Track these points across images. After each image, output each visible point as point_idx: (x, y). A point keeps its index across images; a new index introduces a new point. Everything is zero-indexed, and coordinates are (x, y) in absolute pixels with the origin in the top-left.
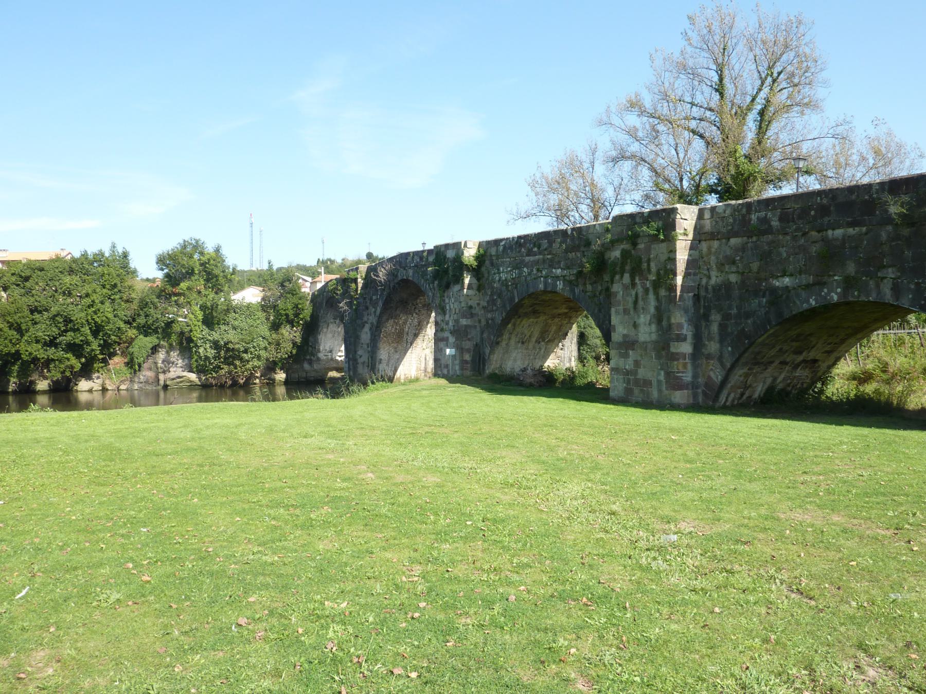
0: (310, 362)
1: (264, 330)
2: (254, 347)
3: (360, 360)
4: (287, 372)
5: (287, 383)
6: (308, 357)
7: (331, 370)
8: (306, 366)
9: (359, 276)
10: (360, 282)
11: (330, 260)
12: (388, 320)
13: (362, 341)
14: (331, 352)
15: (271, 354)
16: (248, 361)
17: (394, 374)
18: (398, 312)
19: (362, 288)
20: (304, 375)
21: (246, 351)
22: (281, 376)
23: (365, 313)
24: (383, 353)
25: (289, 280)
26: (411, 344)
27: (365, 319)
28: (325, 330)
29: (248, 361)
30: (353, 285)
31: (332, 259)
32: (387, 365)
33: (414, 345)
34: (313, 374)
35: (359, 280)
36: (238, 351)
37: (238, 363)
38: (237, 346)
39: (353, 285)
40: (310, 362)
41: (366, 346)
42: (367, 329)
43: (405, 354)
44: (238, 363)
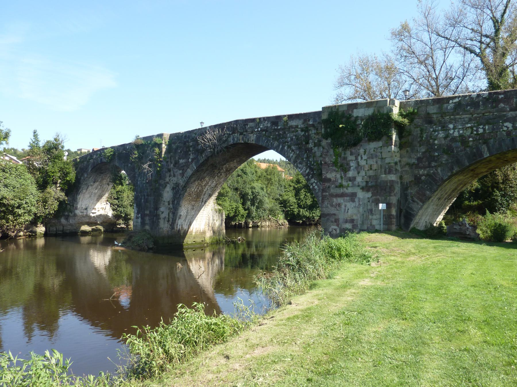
0: (67, 218)
1: (33, 189)
2: (26, 203)
3: (162, 216)
4: (46, 226)
5: (46, 235)
6: (66, 214)
7: (84, 225)
8: (63, 221)
9: (163, 142)
10: (164, 147)
11: (13, 149)
12: (195, 181)
13: (164, 199)
14: (86, 209)
15: (40, 211)
16: (20, 215)
17: (189, 228)
18: (205, 174)
19: (165, 153)
20: (61, 228)
21: (19, 207)
22: (41, 229)
23: (168, 175)
24: (183, 211)
25: (56, 148)
26: (205, 203)
27: (167, 180)
28: (84, 191)
29: (20, 215)
30: (157, 150)
31: (15, 148)
32: (185, 220)
33: (207, 203)
34: (69, 227)
35: (163, 145)
36: (13, 207)
37: (11, 217)
38: (12, 202)
39: (157, 150)
40: (67, 218)
41: (167, 204)
42: (168, 189)
43: (199, 211)
44: (11, 217)
